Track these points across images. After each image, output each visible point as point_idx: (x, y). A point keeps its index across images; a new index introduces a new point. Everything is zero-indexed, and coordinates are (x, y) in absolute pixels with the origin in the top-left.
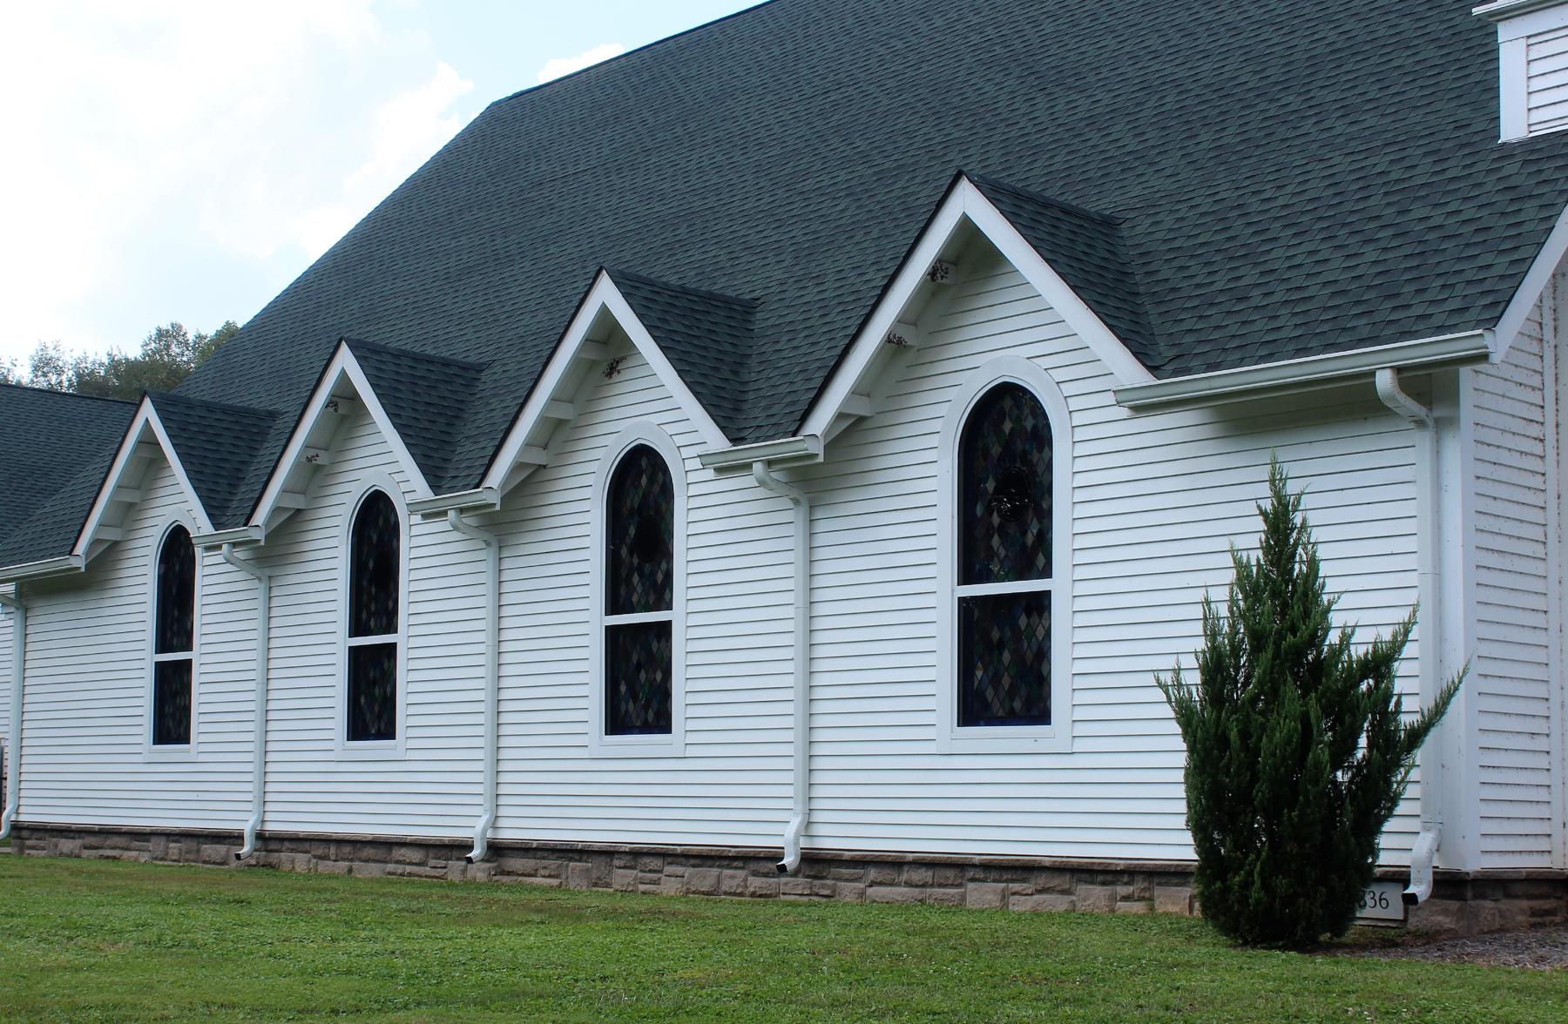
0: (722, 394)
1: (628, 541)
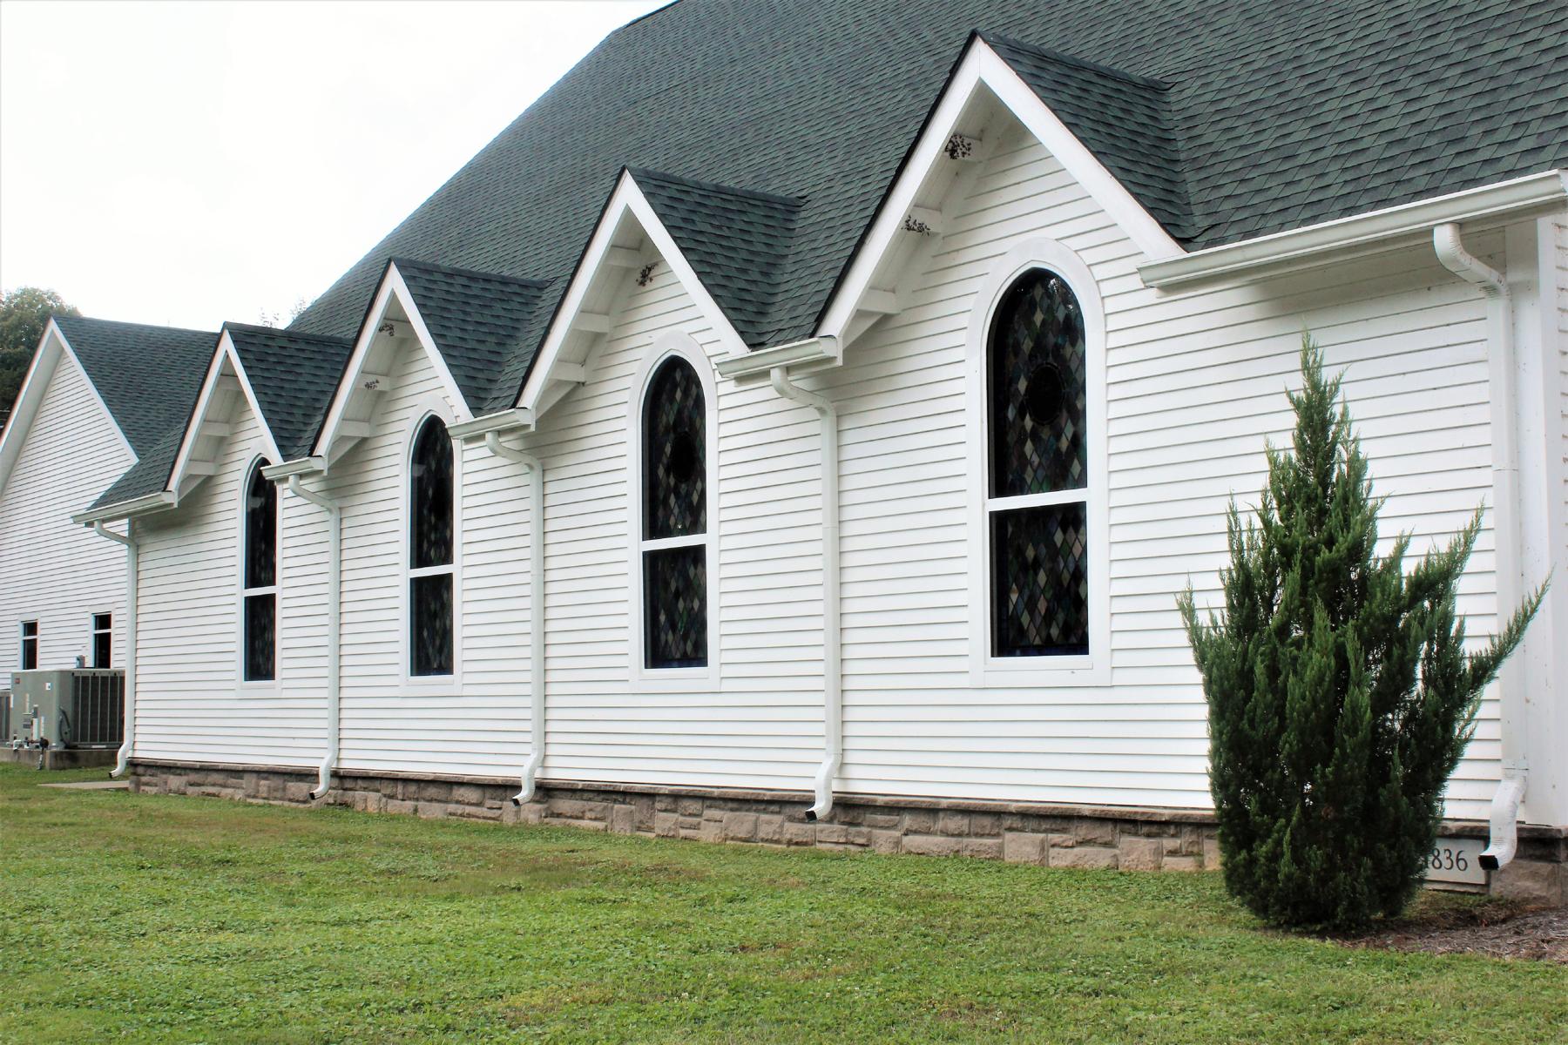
0: (747, 297)
1: (665, 460)
